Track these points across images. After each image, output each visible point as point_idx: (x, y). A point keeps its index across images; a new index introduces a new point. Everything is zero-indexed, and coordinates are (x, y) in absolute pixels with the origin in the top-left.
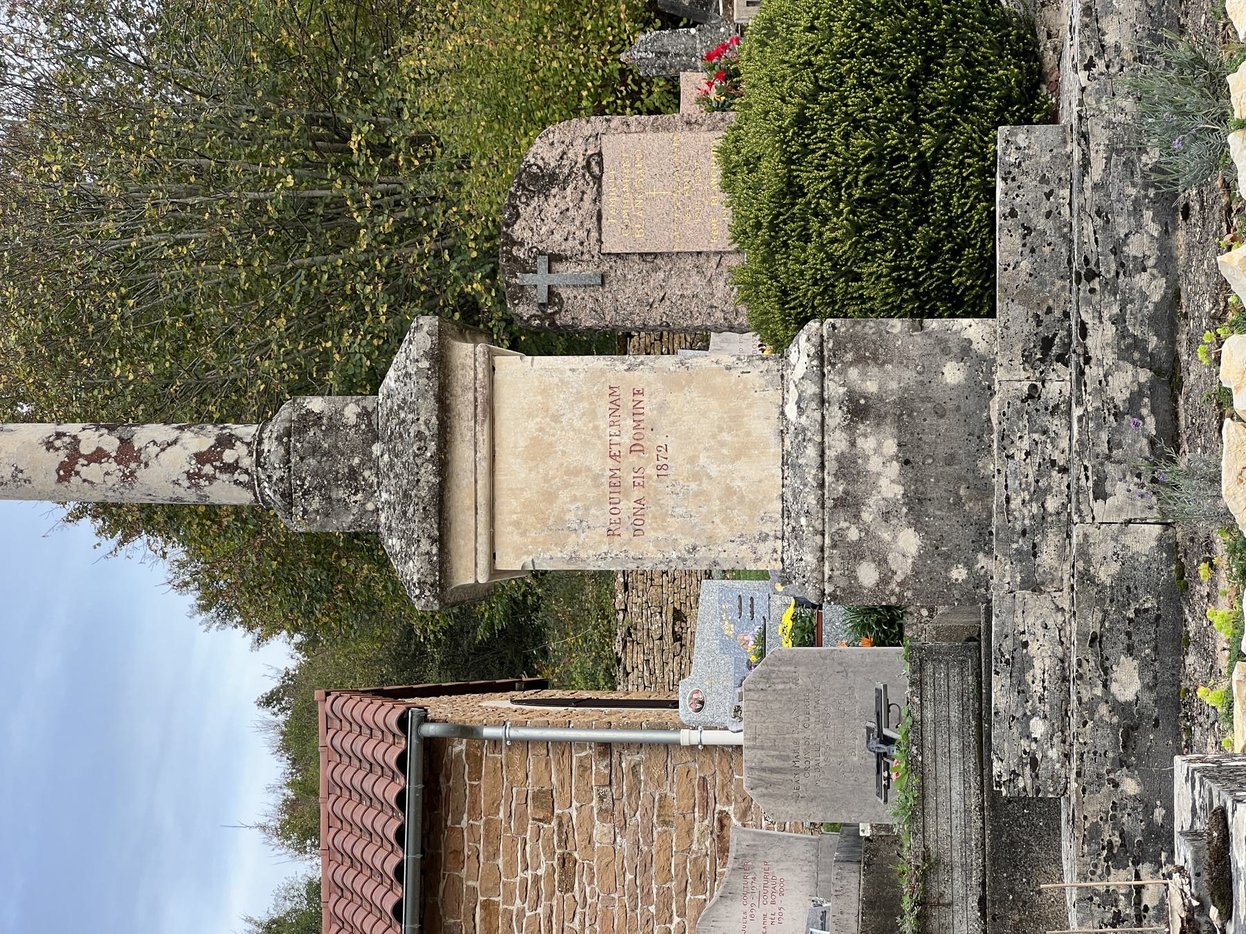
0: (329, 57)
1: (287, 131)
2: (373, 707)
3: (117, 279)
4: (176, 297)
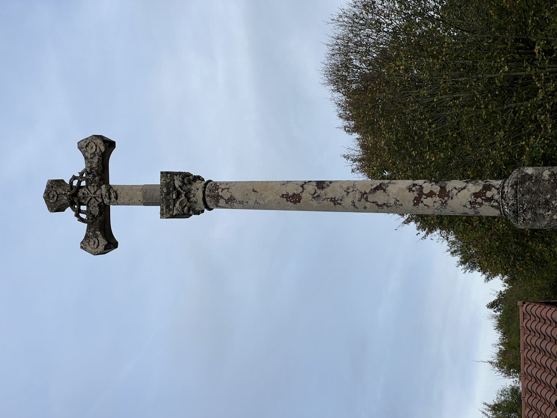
0: (524, 11)
1: (504, 46)
2: (546, 310)
3: (428, 116)
4: (453, 123)
